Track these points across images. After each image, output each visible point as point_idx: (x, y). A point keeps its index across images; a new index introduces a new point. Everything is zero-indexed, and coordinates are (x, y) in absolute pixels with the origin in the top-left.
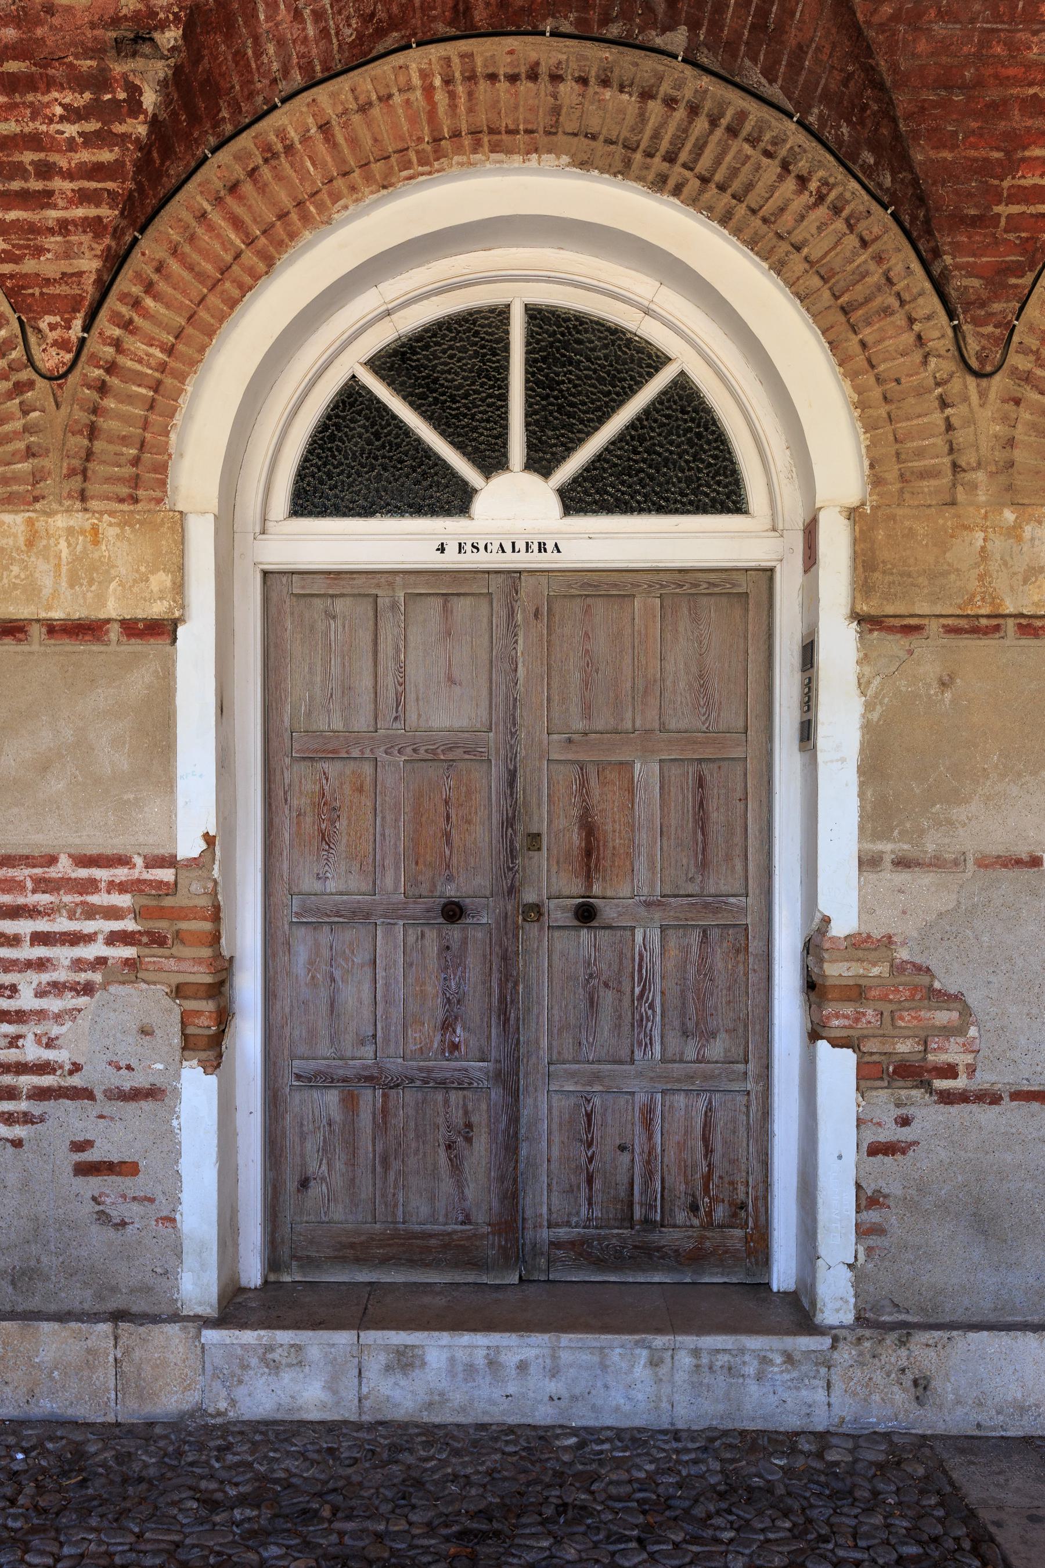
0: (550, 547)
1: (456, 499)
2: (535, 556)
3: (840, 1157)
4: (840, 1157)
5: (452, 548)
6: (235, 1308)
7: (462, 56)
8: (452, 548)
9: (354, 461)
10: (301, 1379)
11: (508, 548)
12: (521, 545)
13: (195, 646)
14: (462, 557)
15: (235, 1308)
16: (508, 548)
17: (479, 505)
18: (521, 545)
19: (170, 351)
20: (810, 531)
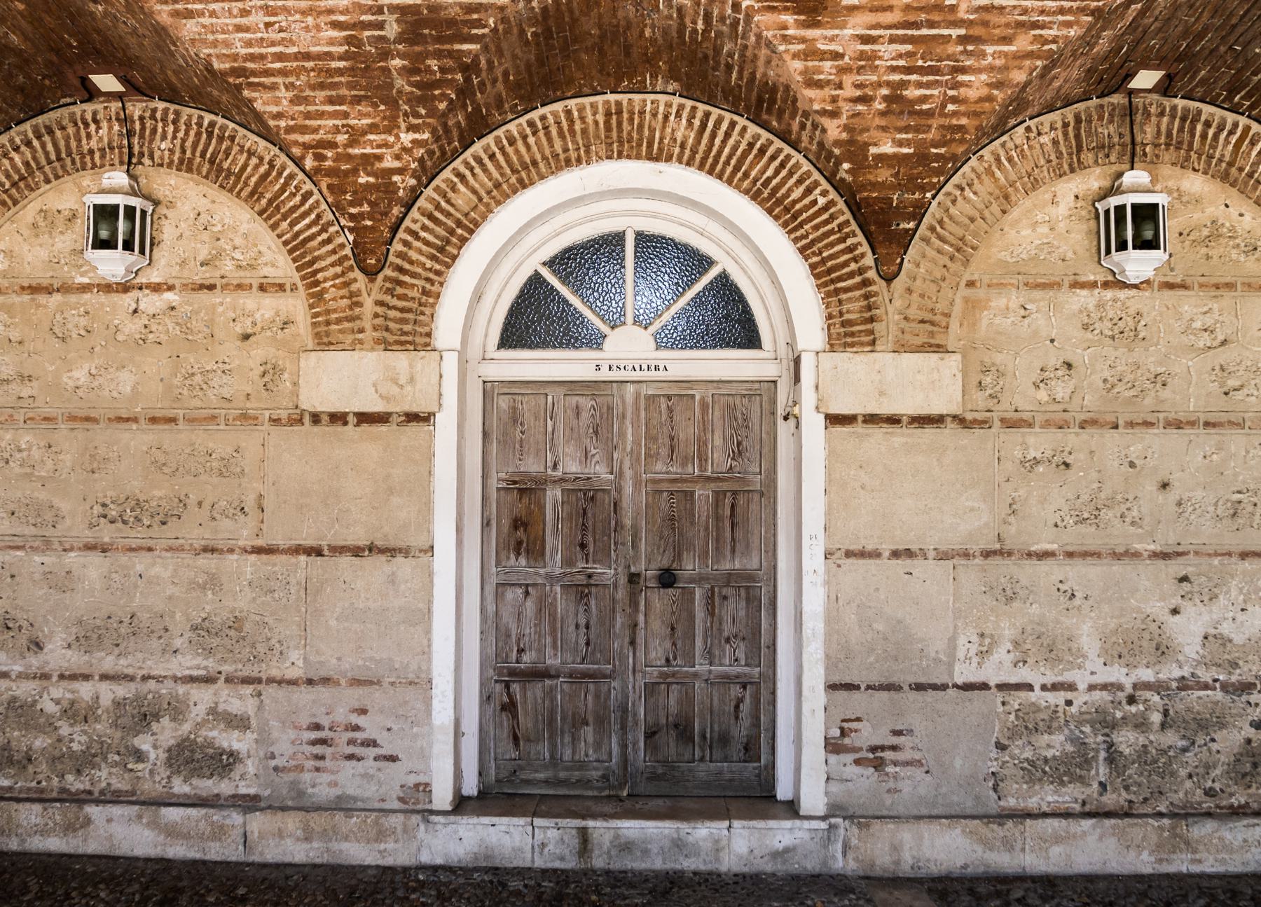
0: (661, 368)
1: (596, 341)
2: (653, 373)
3: (1165, 486)
4: (1165, 486)
5: (605, 368)
6: (461, 805)
7: (652, 103)
8: (605, 368)
9: (534, 318)
10: (511, 839)
11: (637, 368)
12: (645, 367)
13: (446, 422)
14: (649, 373)
15: (461, 805)
16: (637, 368)
17: (607, 344)
18: (645, 367)
19: (14, 184)
20: (797, 361)
